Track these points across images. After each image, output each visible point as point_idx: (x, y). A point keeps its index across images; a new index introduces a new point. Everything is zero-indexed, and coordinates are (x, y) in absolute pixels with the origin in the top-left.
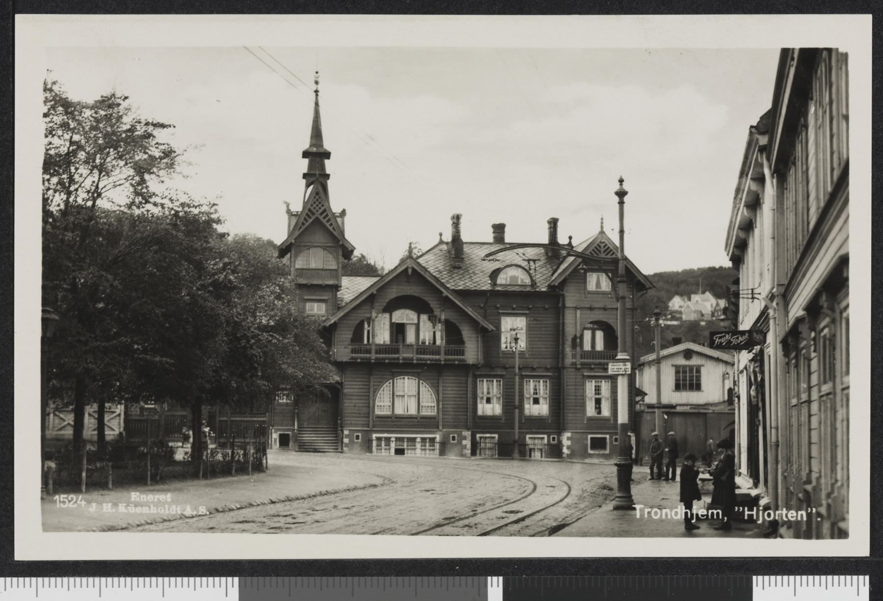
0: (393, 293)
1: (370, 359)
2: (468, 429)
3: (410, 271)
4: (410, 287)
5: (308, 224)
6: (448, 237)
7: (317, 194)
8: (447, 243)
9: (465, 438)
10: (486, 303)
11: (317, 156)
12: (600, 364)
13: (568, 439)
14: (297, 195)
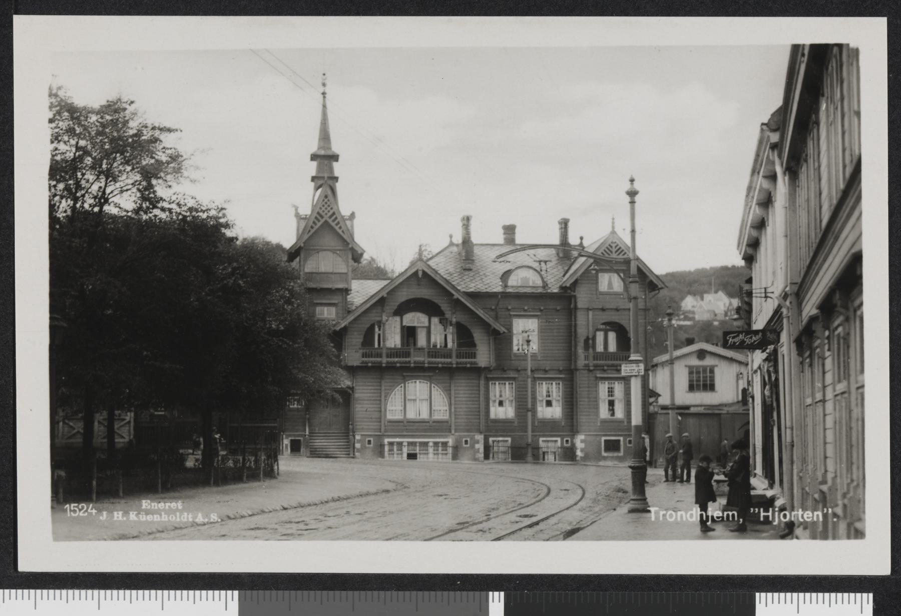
0: (404, 296)
1: (381, 363)
2: (481, 433)
3: (420, 274)
4: (424, 292)
6: (458, 239)
7: (326, 197)
9: (478, 442)
11: (325, 159)
13: (582, 441)
14: (305, 198)
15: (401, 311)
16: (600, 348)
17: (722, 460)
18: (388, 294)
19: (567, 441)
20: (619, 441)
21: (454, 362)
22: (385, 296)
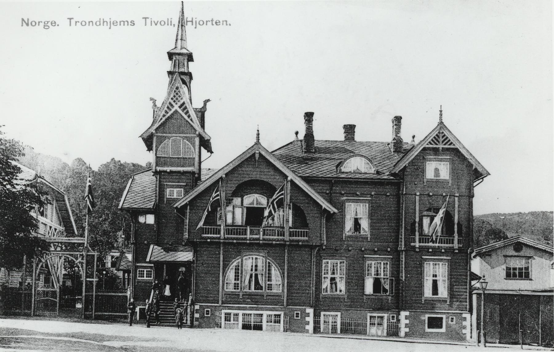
2: (311, 307)
3: (257, 156)
4: (253, 172)
5: (169, 115)
8: (301, 141)
9: (308, 315)
10: (331, 189)
12: (165, 164)
13: (406, 318)
15: (242, 190)
16: (229, 221)
17: (184, 323)
18: (227, 174)
19: (393, 317)
20: (442, 318)
21: (417, 246)
22: (289, 179)
